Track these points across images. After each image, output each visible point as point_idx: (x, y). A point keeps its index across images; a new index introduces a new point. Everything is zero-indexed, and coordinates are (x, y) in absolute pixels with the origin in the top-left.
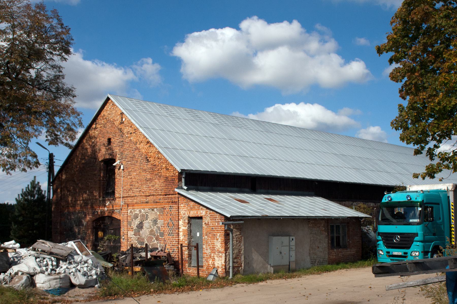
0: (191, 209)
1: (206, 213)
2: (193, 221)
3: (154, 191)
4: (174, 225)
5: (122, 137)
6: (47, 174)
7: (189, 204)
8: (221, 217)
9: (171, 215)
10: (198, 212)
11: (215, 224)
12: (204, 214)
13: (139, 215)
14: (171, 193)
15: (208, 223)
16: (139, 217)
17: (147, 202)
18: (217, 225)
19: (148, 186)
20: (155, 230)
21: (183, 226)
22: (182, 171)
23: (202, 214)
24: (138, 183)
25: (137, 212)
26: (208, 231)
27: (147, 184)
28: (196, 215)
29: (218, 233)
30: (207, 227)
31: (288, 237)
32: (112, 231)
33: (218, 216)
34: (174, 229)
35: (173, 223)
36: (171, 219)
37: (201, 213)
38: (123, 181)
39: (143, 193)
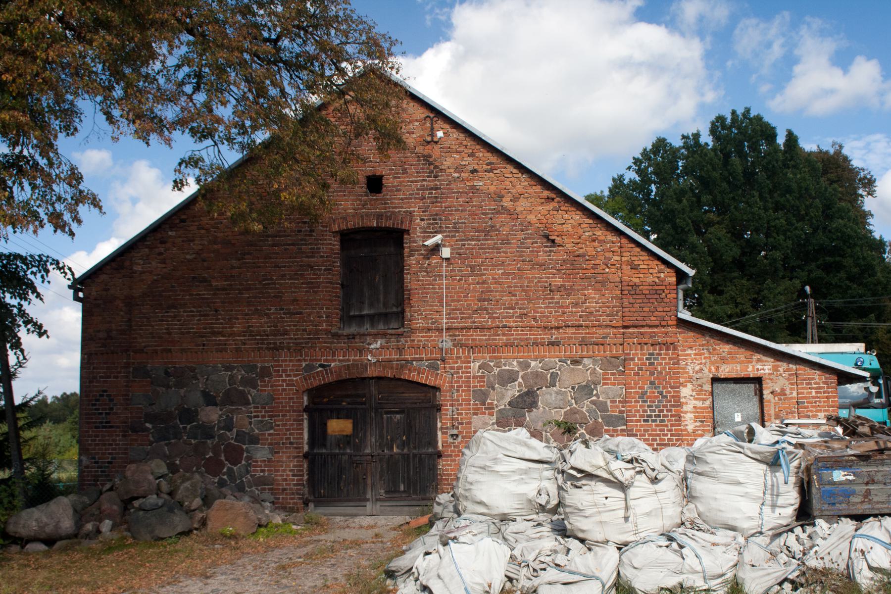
0: (723, 360)
1: (775, 369)
2: (718, 387)
3: (581, 316)
4: (663, 397)
5: (436, 177)
6: (669, 448)
7: (714, 349)
8: (826, 378)
9: (652, 374)
10: (748, 367)
11: (811, 393)
12: (767, 371)
13: (521, 374)
14: (649, 322)
15: (783, 390)
16: (520, 380)
17: (552, 344)
18: (814, 394)
19: (558, 303)
20: (584, 410)
21: (696, 399)
22: (94, 291)
23: (762, 372)
24: (515, 295)
25: (515, 366)
26: (785, 408)
27: (553, 298)
28: (743, 374)
29: (820, 411)
30: (780, 399)
31: (77, 276)
32: (398, 416)
33: (816, 377)
34: (665, 406)
35: (661, 393)
36: (652, 383)
37: (758, 370)
38: (446, 288)
39: (536, 321)
